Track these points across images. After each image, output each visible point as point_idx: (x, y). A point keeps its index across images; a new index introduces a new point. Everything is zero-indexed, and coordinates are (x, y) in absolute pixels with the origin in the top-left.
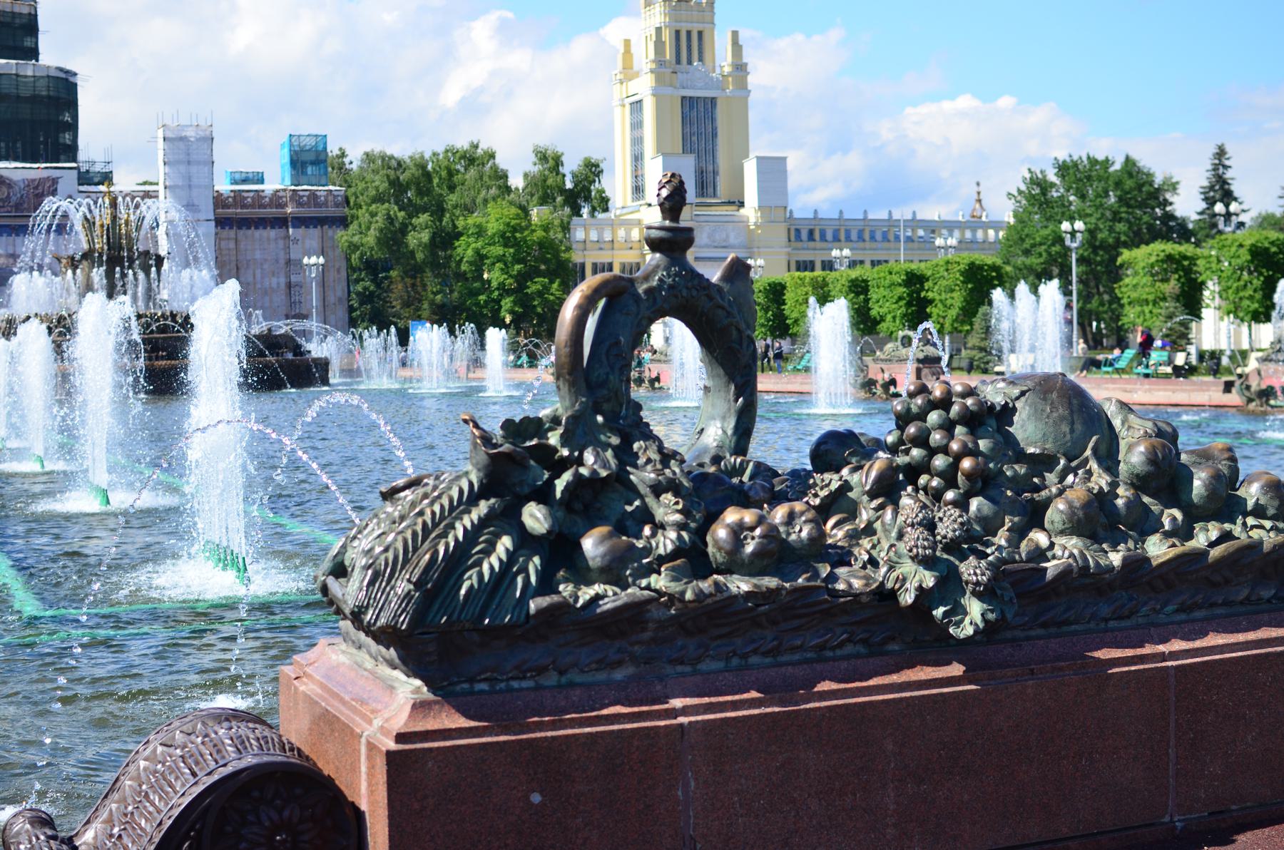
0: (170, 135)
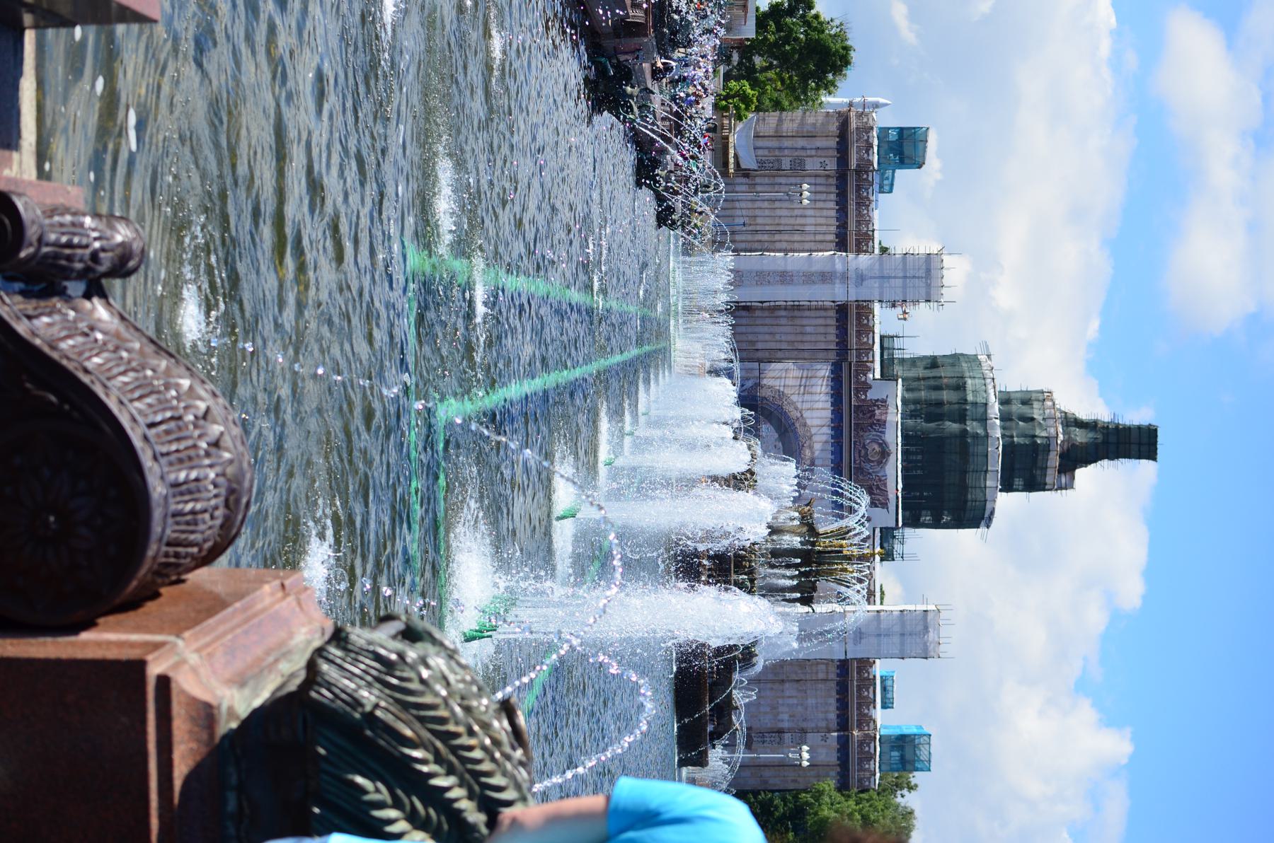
0: (930, 616)
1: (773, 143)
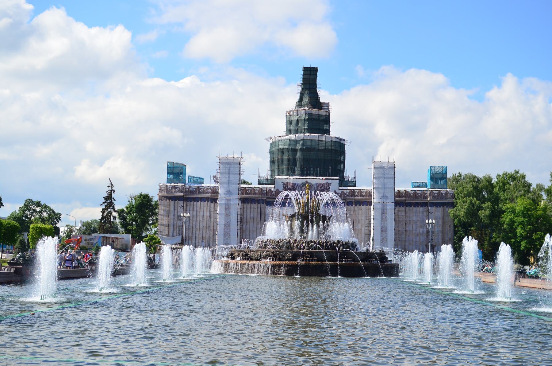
0: (376, 166)
1: (171, 228)
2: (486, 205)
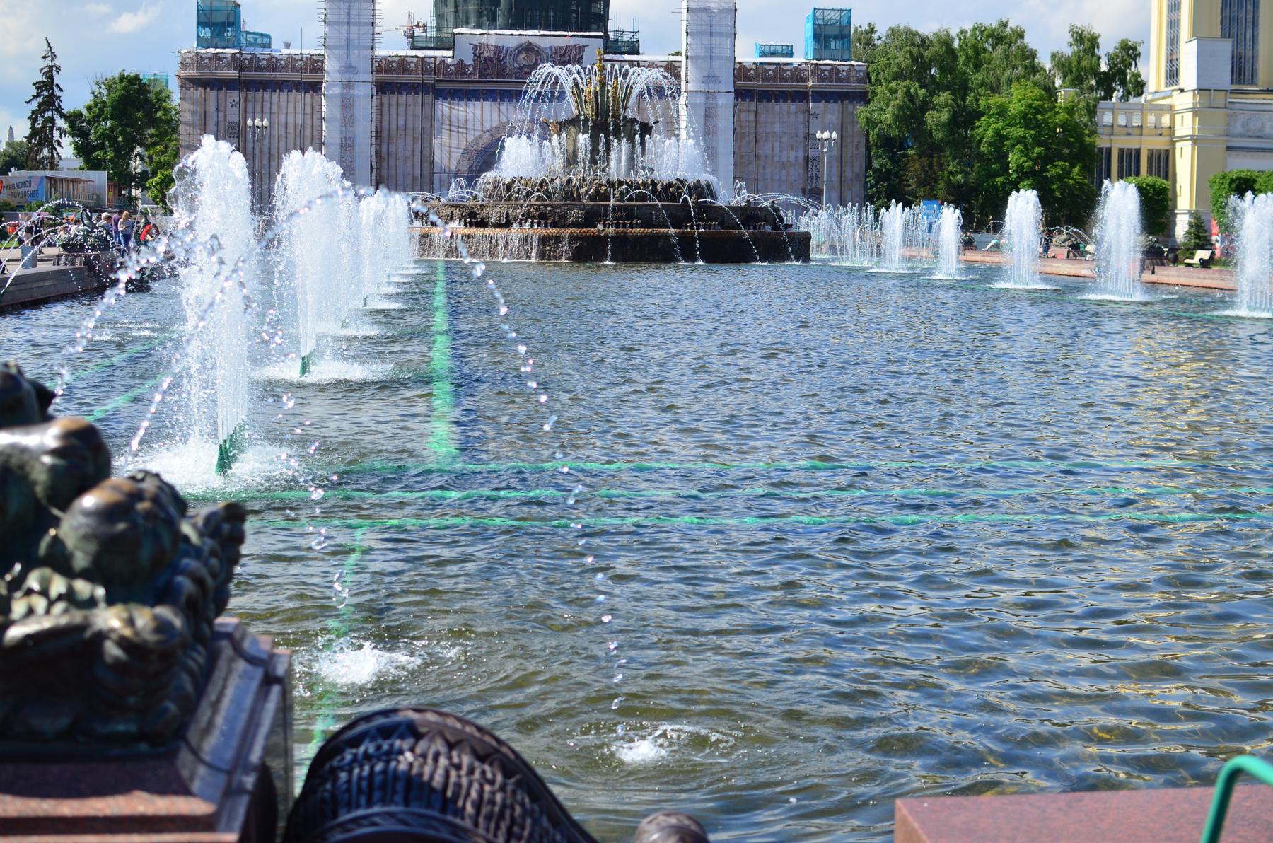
2: (942, 99)
